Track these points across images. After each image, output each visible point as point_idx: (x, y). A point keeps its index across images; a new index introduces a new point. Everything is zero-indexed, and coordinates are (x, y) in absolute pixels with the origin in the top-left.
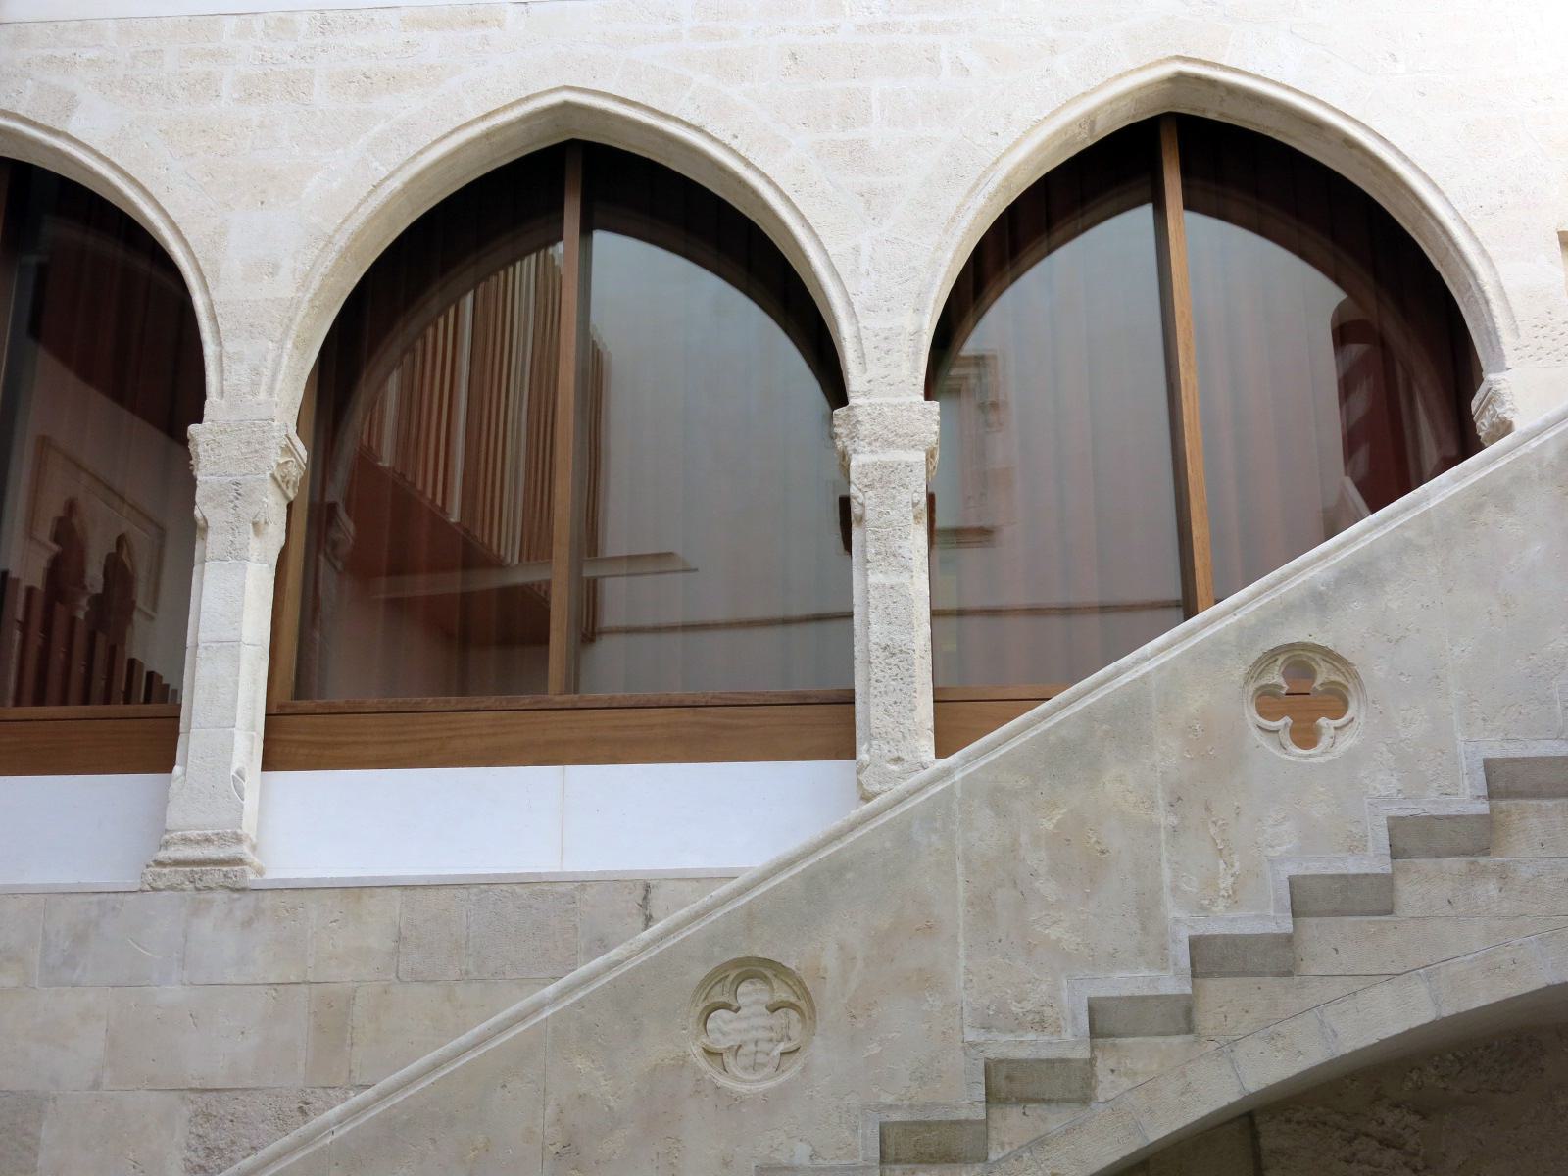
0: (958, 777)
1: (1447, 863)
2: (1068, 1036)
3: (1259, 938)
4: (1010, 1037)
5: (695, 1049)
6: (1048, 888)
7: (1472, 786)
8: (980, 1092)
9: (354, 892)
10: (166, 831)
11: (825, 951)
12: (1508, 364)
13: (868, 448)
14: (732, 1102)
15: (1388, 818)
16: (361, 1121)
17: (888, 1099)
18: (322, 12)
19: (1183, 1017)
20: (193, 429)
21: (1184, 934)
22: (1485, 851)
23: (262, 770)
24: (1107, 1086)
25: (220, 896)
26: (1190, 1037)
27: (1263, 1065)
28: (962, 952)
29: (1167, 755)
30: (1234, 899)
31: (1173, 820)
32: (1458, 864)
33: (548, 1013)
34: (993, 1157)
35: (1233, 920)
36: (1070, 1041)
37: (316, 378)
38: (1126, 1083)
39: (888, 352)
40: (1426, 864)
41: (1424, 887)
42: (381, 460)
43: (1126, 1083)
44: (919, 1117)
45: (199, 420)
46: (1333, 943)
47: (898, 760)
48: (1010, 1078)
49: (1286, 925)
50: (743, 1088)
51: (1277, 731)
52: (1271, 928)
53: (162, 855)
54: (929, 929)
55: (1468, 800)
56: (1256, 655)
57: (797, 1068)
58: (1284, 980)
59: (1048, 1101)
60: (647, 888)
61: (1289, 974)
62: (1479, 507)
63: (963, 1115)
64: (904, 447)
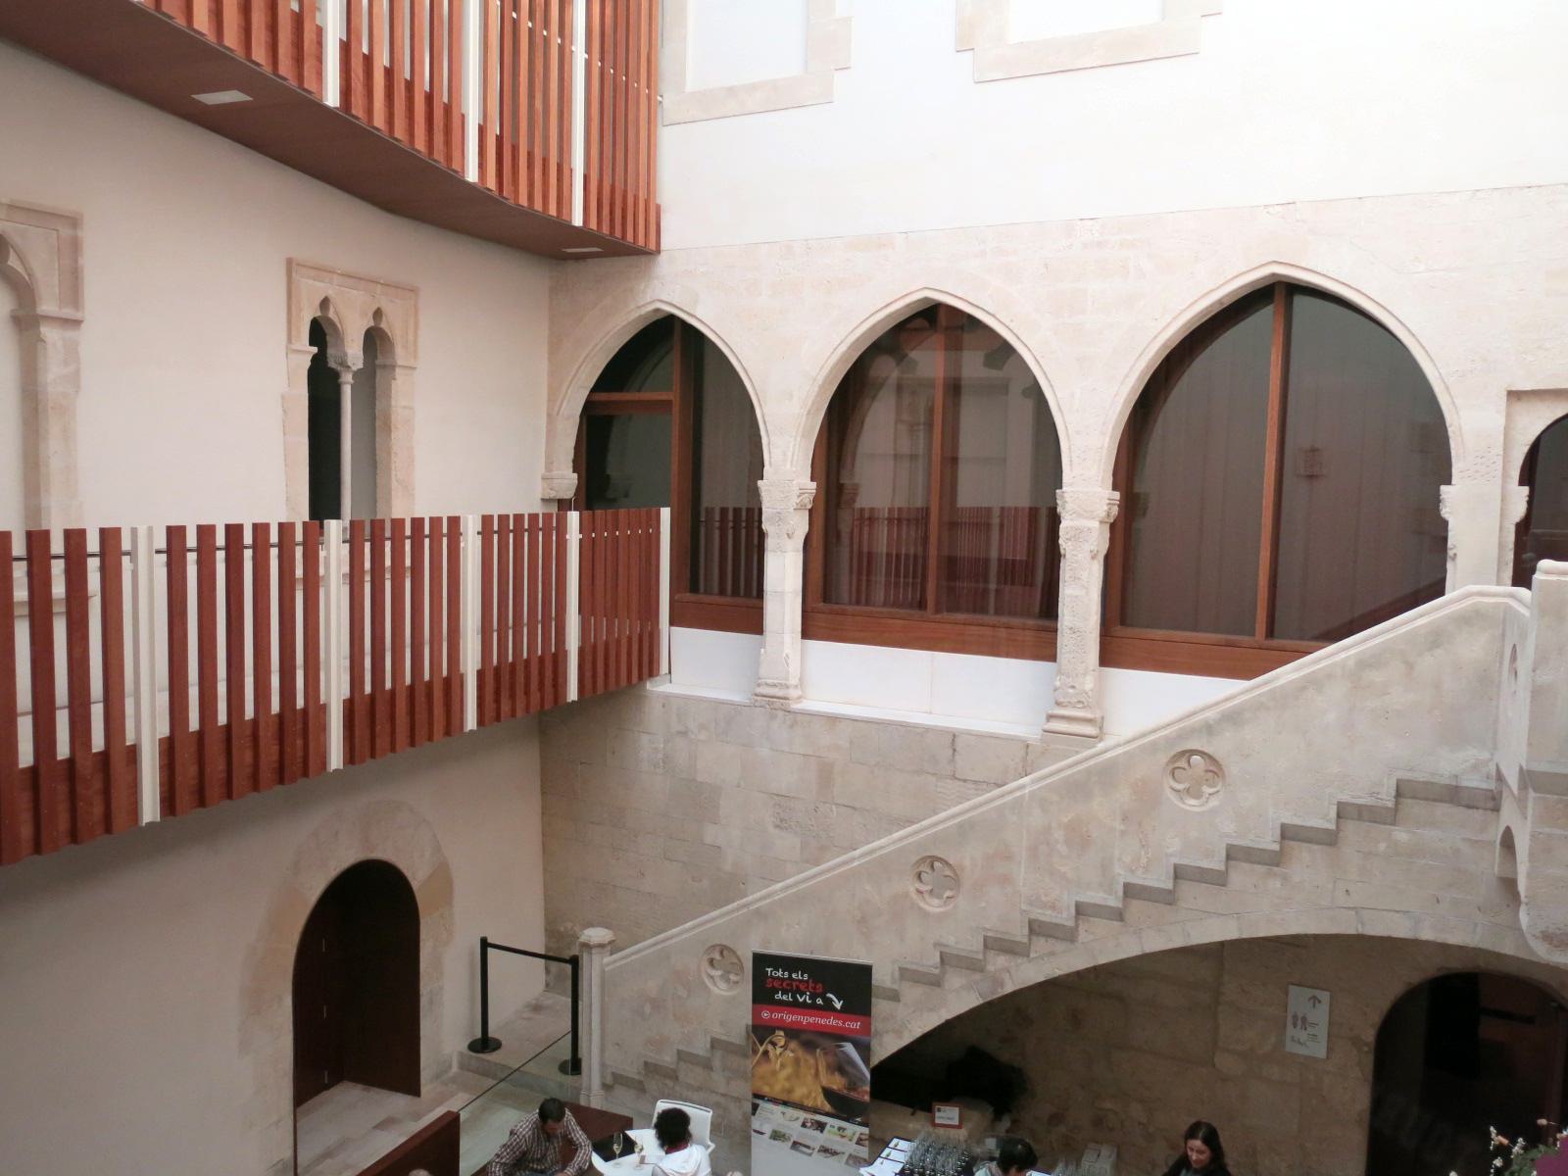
1: (1257, 867)
2: (1065, 915)
3: (1157, 889)
4: (1040, 911)
5: (912, 889)
6: (1062, 848)
7: (1273, 836)
8: (1026, 931)
9: (833, 720)
10: (760, 678)
11: (968, 857)
12: (1453, 482)
13: (1070, 517)
14: (926, 915)
15: (1228, 845)
16: (789, 892)
18: (806, 240)
19: (1119, 915)
20: (760, 482)
21: (1122, 881)
22: (1277, 865)
23: (802, 638)
25: (780, 714)
26: (1122, 923)
27: (1156, 942)
28: (1023, 870)
29: (1123, 795)
30: (1146, 869)
31: (1122, 827)
33: (856, 863)
34: (1032, 956)
35: (1144, 879)
36: (1066, 918)
37: (824, 441)
38: (1091, 937)
39: (1085, 459)
40: (1246, 866)
41: (1242, 877)
43: (1091, 937)
44: (999, 936)
45: (1449, 482)
46: (1193, 895)
47: (1073, 687)
48: (1039, 926)
49: (1169, 885)
51: (1179, 791)
52: (1162, 886)
53: (759, 690)
54: (1008, 857)
55: (1269, 842)
56: (1173, 753)
57: (951, 906)
58: (1169, 907)
59: (1057, 938)
60: (954, 736)
61: (1170, 904)
62: (1304, 688)
63: (1018, 939)
64: (1086, 518)
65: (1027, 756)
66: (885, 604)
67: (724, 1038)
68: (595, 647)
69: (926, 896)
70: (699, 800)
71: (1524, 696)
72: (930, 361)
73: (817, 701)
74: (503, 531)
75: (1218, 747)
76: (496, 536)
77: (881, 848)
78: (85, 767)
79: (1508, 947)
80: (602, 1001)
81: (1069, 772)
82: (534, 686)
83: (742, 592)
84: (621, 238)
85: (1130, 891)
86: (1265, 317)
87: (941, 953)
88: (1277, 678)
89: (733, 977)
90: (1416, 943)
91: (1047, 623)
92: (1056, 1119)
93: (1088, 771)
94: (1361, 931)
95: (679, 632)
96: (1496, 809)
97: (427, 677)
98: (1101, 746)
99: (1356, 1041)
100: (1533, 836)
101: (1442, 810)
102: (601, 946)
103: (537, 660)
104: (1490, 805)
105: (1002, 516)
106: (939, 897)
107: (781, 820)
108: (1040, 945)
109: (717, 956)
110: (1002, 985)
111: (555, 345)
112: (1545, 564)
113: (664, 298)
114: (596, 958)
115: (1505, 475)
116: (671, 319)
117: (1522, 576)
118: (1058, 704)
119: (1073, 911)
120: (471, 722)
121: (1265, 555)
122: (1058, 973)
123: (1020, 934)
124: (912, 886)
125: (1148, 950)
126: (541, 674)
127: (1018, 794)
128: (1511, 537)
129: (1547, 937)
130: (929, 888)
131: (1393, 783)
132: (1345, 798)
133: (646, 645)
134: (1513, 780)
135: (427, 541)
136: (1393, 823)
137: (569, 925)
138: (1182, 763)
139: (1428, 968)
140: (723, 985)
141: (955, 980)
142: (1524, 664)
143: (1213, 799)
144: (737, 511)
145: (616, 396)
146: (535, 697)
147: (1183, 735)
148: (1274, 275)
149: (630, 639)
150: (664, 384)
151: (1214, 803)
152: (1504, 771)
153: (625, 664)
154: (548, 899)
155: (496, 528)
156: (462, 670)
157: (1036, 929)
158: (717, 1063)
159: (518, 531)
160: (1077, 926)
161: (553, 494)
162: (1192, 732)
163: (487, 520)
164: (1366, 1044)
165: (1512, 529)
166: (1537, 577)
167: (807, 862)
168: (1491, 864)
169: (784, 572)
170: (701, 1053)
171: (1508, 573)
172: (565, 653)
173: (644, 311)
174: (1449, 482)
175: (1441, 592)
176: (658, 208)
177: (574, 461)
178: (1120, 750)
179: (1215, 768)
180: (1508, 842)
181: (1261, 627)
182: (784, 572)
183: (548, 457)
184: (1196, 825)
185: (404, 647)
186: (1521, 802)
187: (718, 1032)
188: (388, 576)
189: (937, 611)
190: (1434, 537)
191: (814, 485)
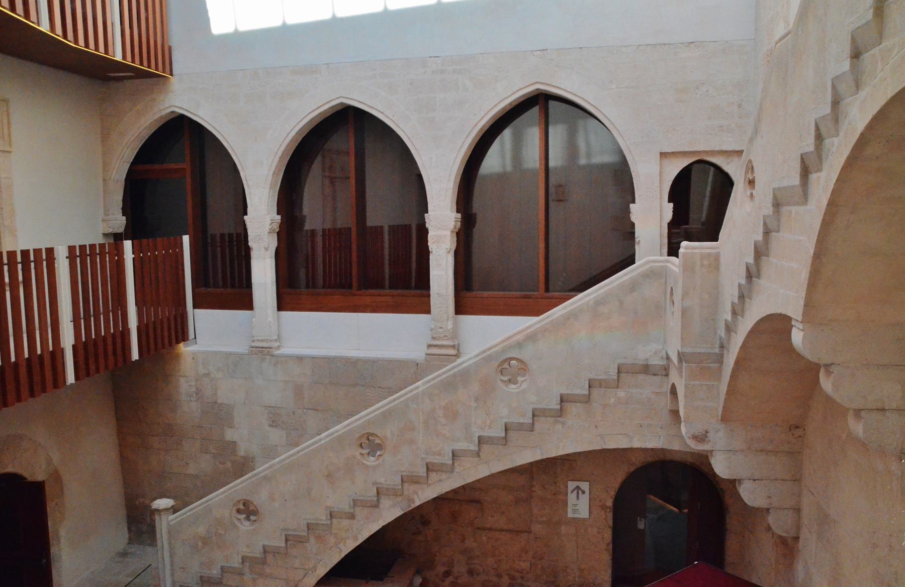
0: (420, 390)
5: (357, 454)
6: (444, 421)
8: (425, 470)
9: (300, 359)
11: (388, 432)
14: (367, 467)
17: (403, 469)
21: (477, 435)
22: (560, 416)
24: (458, 469)
32: (552, 419)
42: (231, 426)
43: (462, 468)
45: (634, 202)
50: (368, 463)
65: (417, 370)
66: (324, 287)
67: (250, 555)
68: (147, 325)
69: (366, 456)
70: (219, 414)
71: (678, 314)
72: (344, 141)
73: (290, 348)
74: (93, 255)
75: (526, 354)
76: (78, 259)
77: (337, 431)
78: (118, 334)
79: (676, 446)
80: (170, 543)
81: (443, 377)
82: (110, 352)
83: (237, 285)
84: (146, 70)
85: (481, 441)
86: (531, 120)
87: (377, 489)
88: (554, 313)
89: (252, 518)
90: (631, 450)
91: (424, 292)
92: (447, 573)
93: (454, 375)
94: (604, 447)
95: (200, 312)
96: (667, 375)
97: (39, 352)
98: (459, 361)
99: (604, 507)
100: (686, 386)
101: (641, 377)
102: (166, 510)
103: (24, 364)
104: (664, 373)
105: (324, 236)
106: (374, 456)
107: (273, 421)
108: (434, 476)
109: (241, 507)
110: (413, 502)
111: (105, 136)
112: (684, 244)
113: (177, 104)
114: (164, 518)
115: (661, 198)
116: (182, 117)
117: (673, 251)
118: (433, 338)
119: (451, 455)
120: (71, 378)
121: (542, 245)
122: (444, 491)
123: (422, 471)
124: (357, 452)
125: (494, 471)
126: (169, 324)
127: (415, 392)
128: (666, 231)
129: (695, 438)
130: (367, 451)
131: (616, 366)
132: (592, 376)
133: (179, 321)
134: (675, 359)
135: (32, 265)
136: (617, 387)
137: (142, 500)
138: (506, 366)
139: (638, 461)
140: (247, 523)
141: (385, 503)
142: (678, 296)
143: (524, 383)
144: (230, 235)
145: (148, 167)
146: (111, 358)
147: (504, 351)
148: (538, 89)
149: (169, 319)
150: (180, 163)
151: (525, 386)
152: (670, 354)
153: (165, 332)
154: (126, 483)
155: (78, 254)
156: (62, 346)
157: (429, 468)
158: (246, 570)
159: (93, 255)
160: (453, 463)
161: (110, 231)
162: (510, 347)
163: (71, 249)
164: (608, 507)
165: (666, 226)
166: (681, 251)
167: (291, 445)
168: (665, 402)
169: (263, 272)
170: (237, 565)
171: (665, 250)
172: (128, 331)
173: (164, 113)
174: (634, 202)
175: (634, 263)
176: (170, 48)
177: (122, 209)
178: (472, 362)
179: (524, 367)
180: (673, 391)
181: (542, 285)
182: (263, 272)
183: (105, 207)
184: (513, 401)
185: (22, 334)
186: (680, 369)
187: (245, 551)
188: (7, 288)
189: (359, 289)
190: (629, 233)
191: (279, 217)
